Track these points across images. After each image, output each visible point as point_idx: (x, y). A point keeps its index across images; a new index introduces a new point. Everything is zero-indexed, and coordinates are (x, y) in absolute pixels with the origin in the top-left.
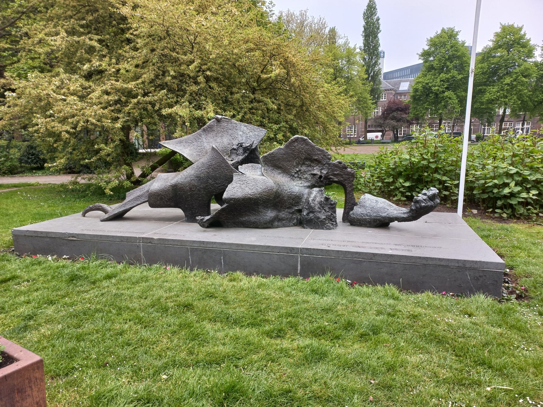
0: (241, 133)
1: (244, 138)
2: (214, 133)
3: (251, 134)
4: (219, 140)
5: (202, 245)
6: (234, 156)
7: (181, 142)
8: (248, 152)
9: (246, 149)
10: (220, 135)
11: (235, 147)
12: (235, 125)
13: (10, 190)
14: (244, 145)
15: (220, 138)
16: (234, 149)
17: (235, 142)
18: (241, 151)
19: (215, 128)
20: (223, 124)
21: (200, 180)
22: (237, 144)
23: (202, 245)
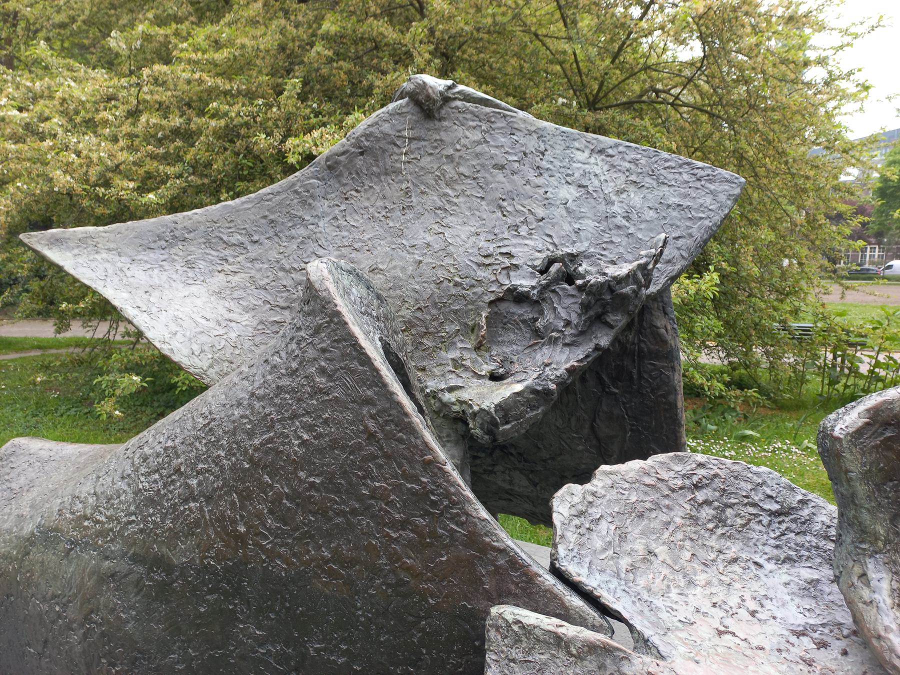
0: (568, 193)
1: (589, 225)
2: (393, 189)
3: (635, 198)
4: (420, 233)
5: (589, 359)
6: (511, 346)
7: (172, 240)
8: (618, 319)
9: (602, 301)
10: (434, 198)
11: (525, 282)
12: (532, 144)
13: (23, 355)
14: (590, 273)
15: (429, 220)
16: (517, 297)
17: (529, 250)
18: (565, 309)
19: (400, 158)
20: (460, 131)
21: (163, 590)
22: (539, 259)
23: (589, 359)
